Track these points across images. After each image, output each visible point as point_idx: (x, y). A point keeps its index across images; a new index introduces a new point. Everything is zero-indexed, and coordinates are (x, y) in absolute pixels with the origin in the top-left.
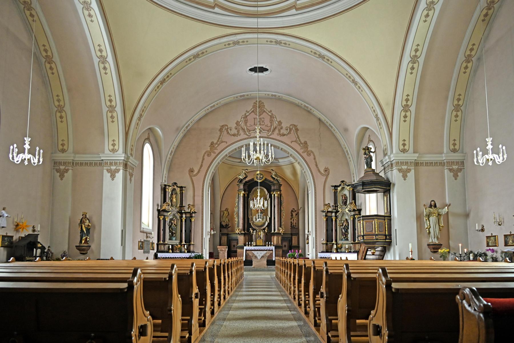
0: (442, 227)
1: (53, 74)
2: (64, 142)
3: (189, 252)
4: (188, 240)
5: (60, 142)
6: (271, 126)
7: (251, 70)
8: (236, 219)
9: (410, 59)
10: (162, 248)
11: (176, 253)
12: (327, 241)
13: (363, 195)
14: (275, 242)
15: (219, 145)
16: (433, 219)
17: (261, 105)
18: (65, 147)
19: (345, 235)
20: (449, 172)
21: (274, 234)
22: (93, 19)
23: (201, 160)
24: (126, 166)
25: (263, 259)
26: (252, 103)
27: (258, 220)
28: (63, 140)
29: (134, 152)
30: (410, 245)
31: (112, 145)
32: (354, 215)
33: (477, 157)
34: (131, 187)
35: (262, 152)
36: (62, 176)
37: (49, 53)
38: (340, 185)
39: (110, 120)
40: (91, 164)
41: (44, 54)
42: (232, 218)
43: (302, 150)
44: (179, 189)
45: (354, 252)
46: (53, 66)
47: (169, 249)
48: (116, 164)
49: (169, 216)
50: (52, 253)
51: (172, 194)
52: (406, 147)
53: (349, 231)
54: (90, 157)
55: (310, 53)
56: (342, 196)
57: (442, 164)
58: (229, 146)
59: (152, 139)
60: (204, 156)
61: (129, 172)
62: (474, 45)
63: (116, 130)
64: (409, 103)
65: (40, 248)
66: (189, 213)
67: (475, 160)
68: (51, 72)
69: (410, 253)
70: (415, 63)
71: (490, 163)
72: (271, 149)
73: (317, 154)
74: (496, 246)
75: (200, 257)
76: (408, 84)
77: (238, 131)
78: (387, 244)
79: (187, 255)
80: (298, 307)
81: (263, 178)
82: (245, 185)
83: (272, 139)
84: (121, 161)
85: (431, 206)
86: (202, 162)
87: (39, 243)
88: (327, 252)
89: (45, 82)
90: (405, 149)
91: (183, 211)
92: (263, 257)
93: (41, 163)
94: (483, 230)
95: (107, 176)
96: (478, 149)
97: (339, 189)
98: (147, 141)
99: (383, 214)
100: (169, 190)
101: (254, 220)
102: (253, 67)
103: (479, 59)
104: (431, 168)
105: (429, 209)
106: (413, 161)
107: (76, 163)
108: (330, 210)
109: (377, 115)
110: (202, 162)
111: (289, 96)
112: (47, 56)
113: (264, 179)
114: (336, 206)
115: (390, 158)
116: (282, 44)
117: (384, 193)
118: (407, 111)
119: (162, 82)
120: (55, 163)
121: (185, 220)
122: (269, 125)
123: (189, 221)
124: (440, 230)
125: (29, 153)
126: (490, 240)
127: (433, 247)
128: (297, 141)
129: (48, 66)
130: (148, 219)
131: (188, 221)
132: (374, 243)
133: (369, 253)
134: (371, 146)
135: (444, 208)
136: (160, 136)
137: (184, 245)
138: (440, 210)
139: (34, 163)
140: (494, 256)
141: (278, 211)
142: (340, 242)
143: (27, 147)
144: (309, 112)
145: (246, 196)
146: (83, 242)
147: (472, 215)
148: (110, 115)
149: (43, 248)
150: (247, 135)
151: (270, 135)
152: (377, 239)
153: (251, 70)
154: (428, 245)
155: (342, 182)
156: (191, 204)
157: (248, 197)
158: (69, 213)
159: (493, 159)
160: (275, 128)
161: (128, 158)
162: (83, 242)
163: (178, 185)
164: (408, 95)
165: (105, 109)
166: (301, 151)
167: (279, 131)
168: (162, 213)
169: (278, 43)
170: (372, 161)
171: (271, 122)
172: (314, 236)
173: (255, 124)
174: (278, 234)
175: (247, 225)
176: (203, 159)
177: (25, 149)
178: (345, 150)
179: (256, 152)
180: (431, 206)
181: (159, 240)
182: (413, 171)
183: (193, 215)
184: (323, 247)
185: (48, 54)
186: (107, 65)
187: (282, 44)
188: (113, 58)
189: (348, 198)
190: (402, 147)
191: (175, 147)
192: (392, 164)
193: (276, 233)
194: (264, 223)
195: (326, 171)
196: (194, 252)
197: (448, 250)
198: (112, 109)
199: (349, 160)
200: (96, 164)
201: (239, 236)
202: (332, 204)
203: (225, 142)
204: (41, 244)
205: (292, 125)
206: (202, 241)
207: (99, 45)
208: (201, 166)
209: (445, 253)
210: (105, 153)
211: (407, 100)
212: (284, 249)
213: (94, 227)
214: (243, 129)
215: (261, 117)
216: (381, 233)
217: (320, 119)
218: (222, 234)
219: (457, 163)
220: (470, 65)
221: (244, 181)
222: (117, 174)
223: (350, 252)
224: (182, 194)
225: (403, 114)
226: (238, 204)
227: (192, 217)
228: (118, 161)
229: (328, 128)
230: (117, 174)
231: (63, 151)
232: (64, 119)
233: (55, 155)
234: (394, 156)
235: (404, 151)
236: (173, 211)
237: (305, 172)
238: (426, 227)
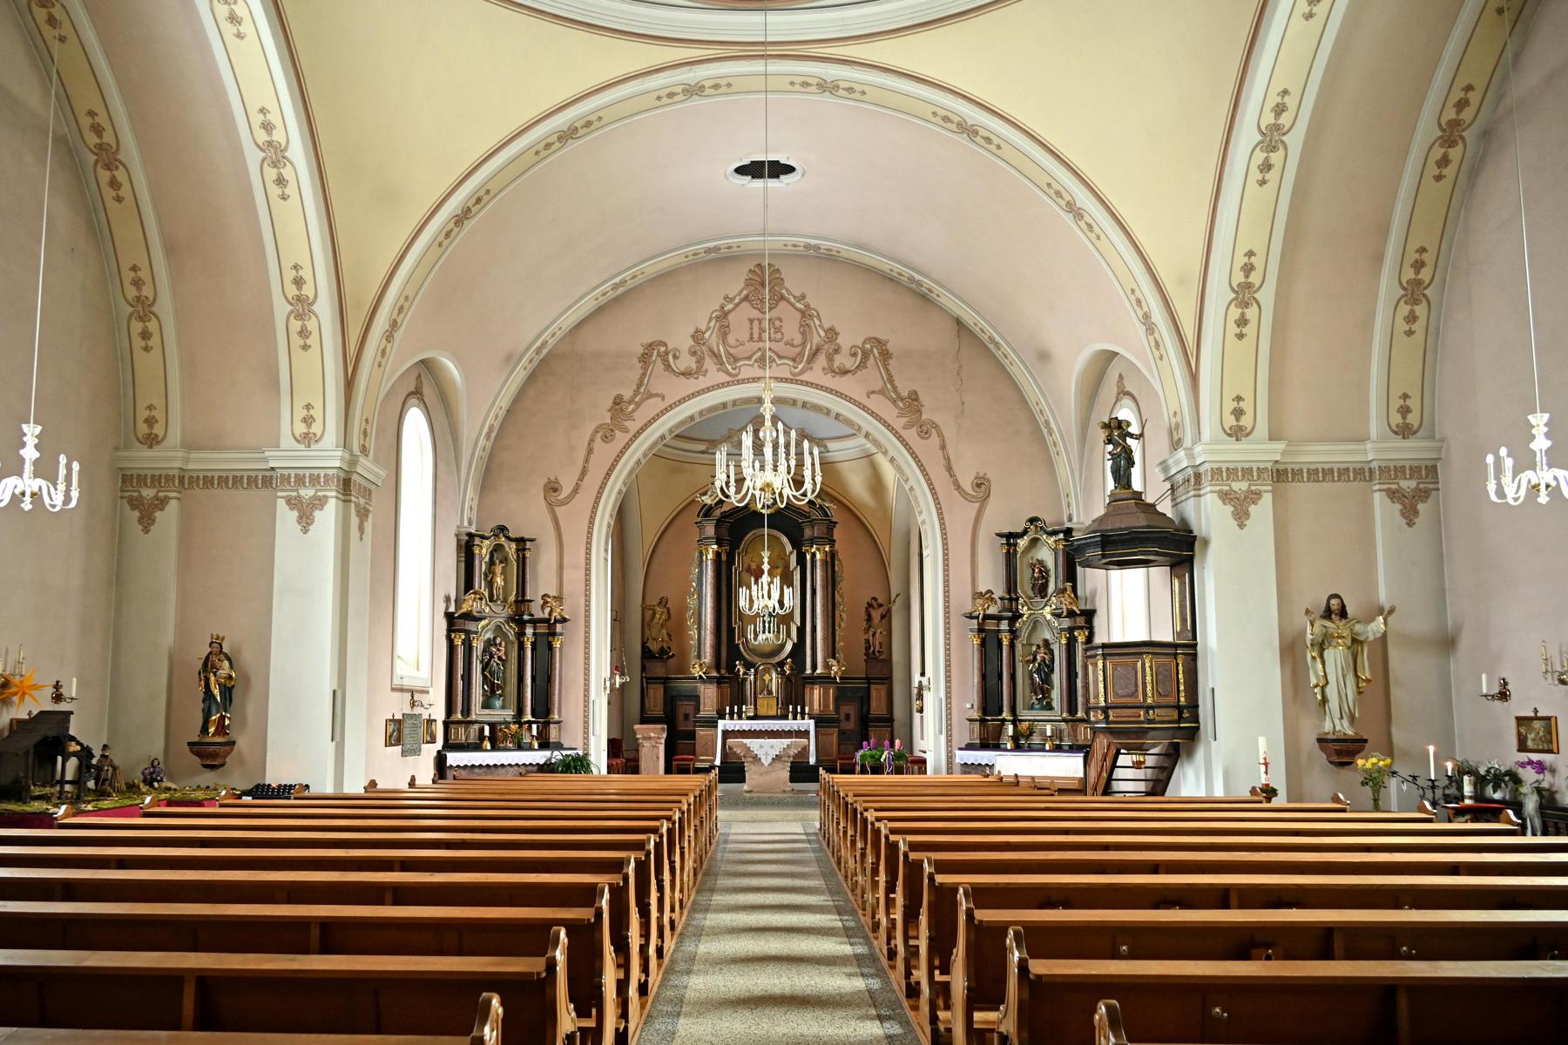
0: (1368, 681)
1: (119, 199)
2: (154, 413)
3: (545, 745)
4: (543, 708)
5: (143, 414)
6: (804, 344)
7: (740, 171)
8: (694, 633)
9: (1259, 138)
10: (460, 735)
11: (506, 749)
12: (985, 709)
13: (1099, 573)
14: (816, 706)
15: (638, 405)
16: (1336, 656)
18: (158, 430)
19: (1042, 690)
21: (813, 680)
22: (242, 29)
24: (346, 485)
25: (778, 765)
27: (761, 637)
28: (150, 408)
29: (371, 444)
30: (1262, 741)
31: (305, 420)
32: (1071, 630)
33: (1498, 478)
34: (361, 551)
35: (782, 468)
36: (147, 521)
37: (108, 138)
38: (1025, 532)
39: (297, 341)
40: (237, 481)
41: (92, 139)
42: (681, 627)
43: (904, 420)
45: (1073, 749)
46: (120, 175)
47: (482, 737)
48: (315, 480)
49: (483, 632)
50: (115, 768)
51: (492, 563)
52: (1246, 421)
53: (1056, 677)
55: (932, 118)
56: (1033, 566)
57: (1362, 474)
58: (671, 407)
59: (428, 391)
60: (592, 440)
61: (357, 505)
62: (1469, 88)
63: (314, 372)
64: (1255, 278)
65: (75, 754)
66: (547, 621)
67: (1492, 487)
68: (114, 193)
69: (1263, 768)
70: (1274, 149)
71: (1543, 498)
72: (811, 453)
73: (949, 433)
74: (1550, 751)
75: (578, 764)
76: (1251, 217)
77: (700, 362)
78: (1183, 732)
79: (540, 757)
80: (905, 1004)
83: (807, 384)
84: (331, 472)
85: (1328, 614)
86: (587, 461)
87: (73, 739)
88: (984, 746)
90: (1241, 428)
91: (526, 617)
92: (777, 758)
93: (73, 504)
94: (1503, 695)
95: (286, 517)
96: (1503, 451)
97: (1022, 543)
98: (414, 400)
99: (1168, 637)
100: (483, 550)
101: (751, 636)
102: (746, 162)
103: (1486, 135)
104: (1326, 486)
105: (1327, 623)
106: (1269, 465)
107: (191, 478)
108: (992, 610)
109: (1147, 316)
110: (587, 461)
111: (860, 247)
112: (100, 146)
114: (1011, 600)
115: (1191, 456)
116: (841, 93)
117: (1172, 566)
118: (1247, 305)
119: (461, 218)
120: (126, 479)
121: (534, 645)
122: (798, 339)
124: (1360, 693)
125: (36, 474)
126: (1531, 729)
127: (1337, 746)
128: (889, 390)
129: (104, 176)
130: (418, 652)
131: (542, 648)
132: (1142, 733)
133: (1123, 760)
134: (1125, 413)
135: (1373, 619)
137: (530, 723)
138: (1358, 628)
139: (54, 506)
140: (1545, 785)
141: (825, 605)
142: (1024, 714)
143: (30, 453)
145: (724, 558)
146: (212, 730)
147: (1464, 643)
148: (296, 325)
149: (85, 754)
151: (801, 373)
152: (1150, 721)
153: (740, 171)
154: (1320, 740)
155: (1032, 520)
156: (553, 593)
157: (731, 561)
158: (168, 638)
159: (1553, 484)
161: (353, 462)
162: (212, 730)
164: (1250, 254)
165: (281, 309)
166: (899, 424)
167: (830, 359)
168: (460, 624)
170: (1131, 463)
171: (805, 330)
172: (942, 695)
173: (751, 338)
174: (825, 680)
176: (590, 451)
177: (23, 460)
178: (1041, 421)
179: (762, 468)
180: (1328, 614)
181: (450, 709)
182: (1267, 499)
183: (559, 628)
184: (972, 732)
185: (105, 140)
186: (287, 172)
187: (841, 93)
188: (304, 144)
189: (1052, 573)
190: (1230, 421)
191: (502, 414)
192: (1198, 476)
193: (819, 677)
194: (783, 646)
195: (979, 485)
196: (559, 746)
197: (1389, 761)
198: (302, 307)
199: (1053, 450)
200: (252, 481)
201: (701, 687)
202: (999, 591)
203: (657, 395)
205: (869, 339)
206: (586, 706)
207: (262, 111)
208: (584, 472)
209: (1380, 770)
210: (283, 445)
212: (846, 726)
213: (246, 680)
214: (716, 356)
215: (775, 313)
216: (1163, 701)
217: (959, 322)
218: (648, 680)
219: (1415, 471)
220: (1455, 153)
221: (718, 513)
222: (317, 513)
223: (1058, 749)
225: (1235, 313)
226: (700, 584)
227: (554, 634)
230: (317, 513)
231: (151, 441)
232: (154, 342)
233: (124, 454)
234: (1209, 447)
235: (1237, 433)
237: (911, 489)
238: (1313, 681)
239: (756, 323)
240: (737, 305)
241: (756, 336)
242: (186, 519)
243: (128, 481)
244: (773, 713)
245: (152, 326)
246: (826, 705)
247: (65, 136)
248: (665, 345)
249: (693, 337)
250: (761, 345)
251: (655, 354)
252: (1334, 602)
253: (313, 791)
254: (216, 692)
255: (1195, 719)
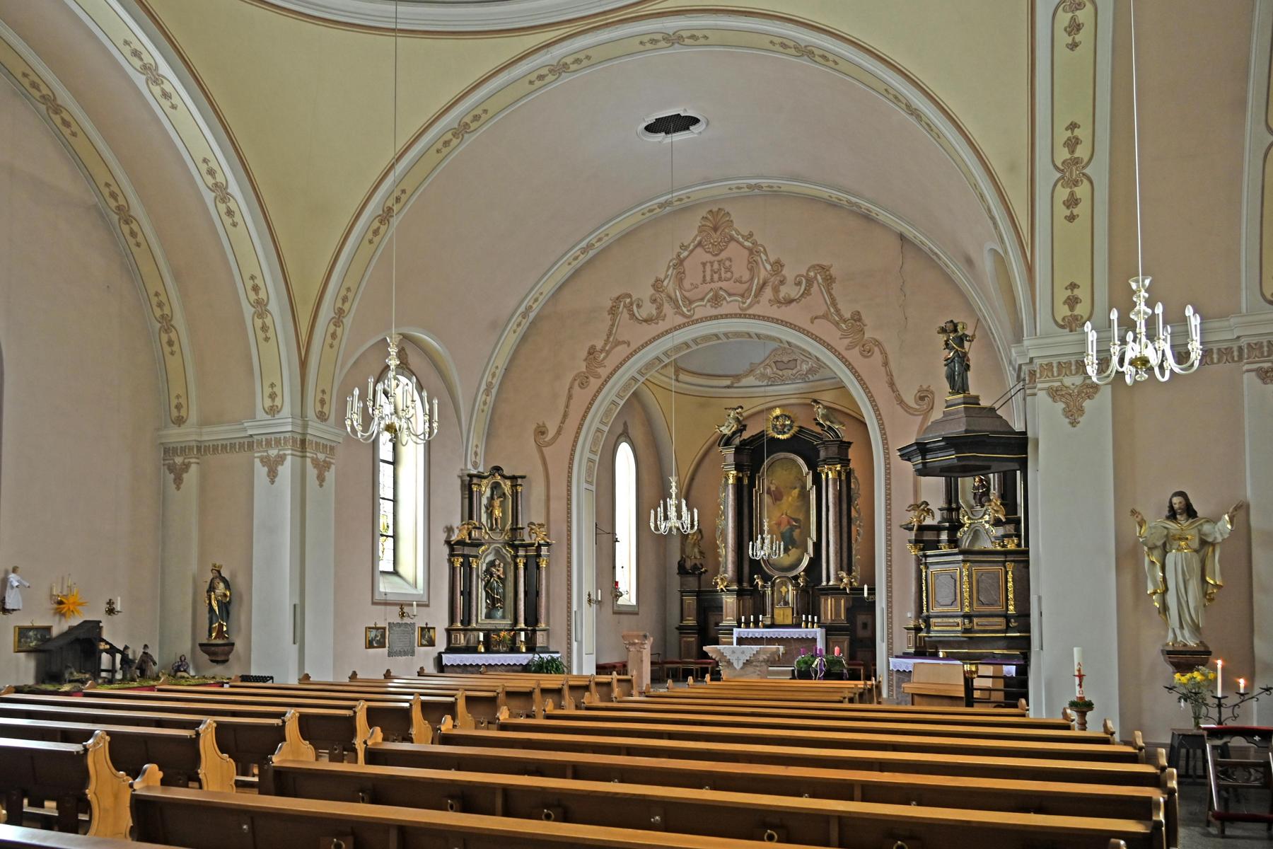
0: (1216, 586)
1: (138, 245)
3: (531, 649)
4: (533, 618)
5: (174, 402)
6: (752, 279)
7: (650, 129)
11: (498, 652)
15: (608, 353)
17: (716, 224)
18: (183, 413)
20: (1258, 381)
23: (563, 400)
26: (696, 220)
30: (1076, 651)
36: (178, 481)
40: (233, 446)
41: (113, 204)
43: (846, 342)
44: (509, 483)
46: (134, 226)
48: (278, 442)
51: (492, 498)
54: (226, 432)
59: (415, 360)
60: (571, 388)
61: (312, 459)
63: (277, 356)
64: (1082, 152)
66: (532, 545)
69: (1077, 680)
77: (659, 308)
81: (791, 427)
82: (738, 451)
83: (754, 317)
84: (288, 435)
86: (567, 407)
89: (131, 271)
92: (748, 663)
108: (929, 521)
110: (567, 407)
111: (796, 180)
112: (118, 208)
113: (795, 429)
121: (525, 565)
122: (746, 276)
123: (533, 566)
128: (832, 314)
129: (126, 229)
136: (437, 351)
138: (1207, 528)
144: (867, 218)
145: (746, 481)
148: (259, 323)
150: (684, 315)
151: (750, 306)
153: (650, 129)
157: (751, 484)
160: (764, 284)
163: (505, 473)
166: (841, 345)
167: (776, 290)
169: (674, 39)
171: (752, 266)
173: (704, 281)
174: (835, 591)
175: (748, 569)
176: (570, 397)
192: (1032, 374)
195: (922, 398)
198: (261, 307)
203: (624, 342)
204: (107, 643)
205: (813, 267)
206: (569, 620)
208: (565, 416)
211: (1072, 144)
215: (723, 255)
217: (902, 237)
221: (737, 441)
222: (280, 468)
224: (515, 495)
228: (282, 436)
229: (930, 260)
231: (180, 421)
236: (494, 541)
239: (708, 267)
240: (692, 252)
241: (708, 278)
242: (203, 477)
243: (169, 451)
244: (789, 621)
245: (173, 335)
246: (838, 614)
247: (95, 206)
248: (630, 296)
249: (653, 286)
250: (713, 285)
251: (621, 305)
252: (1176, 500)
253: (278, 682)
254: (216, 608)
255: (1027, 628)
